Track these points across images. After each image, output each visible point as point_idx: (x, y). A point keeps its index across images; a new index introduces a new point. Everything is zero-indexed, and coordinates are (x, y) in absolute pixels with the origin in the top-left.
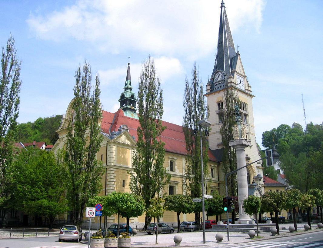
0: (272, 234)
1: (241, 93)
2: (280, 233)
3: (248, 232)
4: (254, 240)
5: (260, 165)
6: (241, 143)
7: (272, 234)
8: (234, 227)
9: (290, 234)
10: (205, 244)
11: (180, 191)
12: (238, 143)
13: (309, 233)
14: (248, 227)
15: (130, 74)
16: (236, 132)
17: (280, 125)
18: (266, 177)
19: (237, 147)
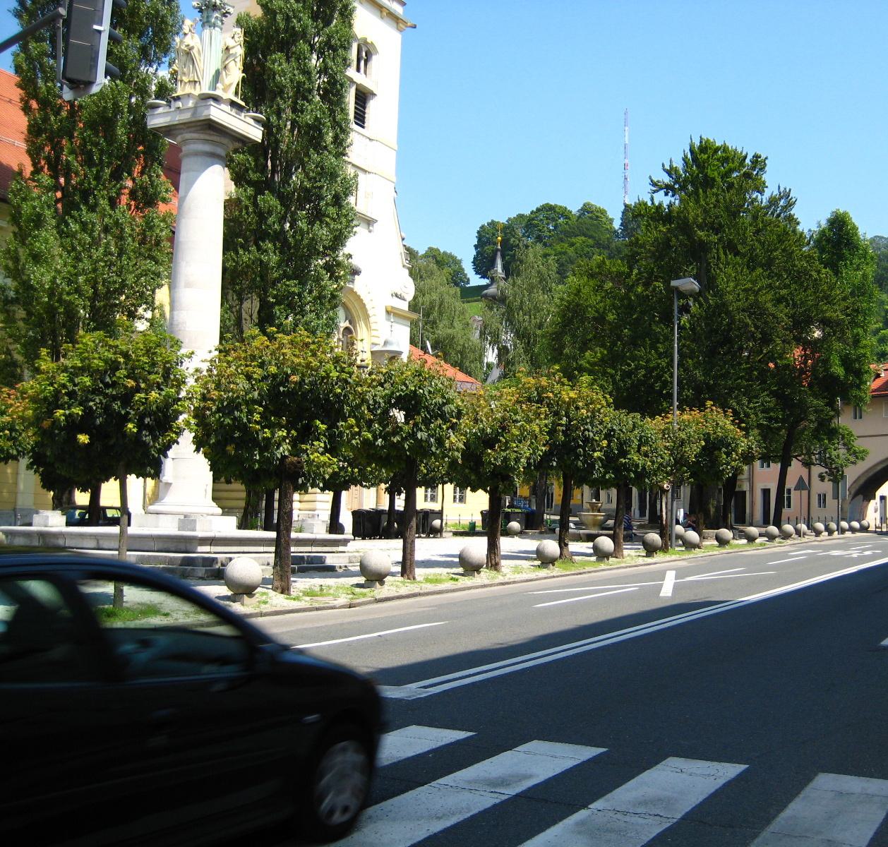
0: (230, 593)
1: (379, 13)
2: (503, 562)
3: (593, 541)
4: (674, 557)
5: (404, 306)
6: (203, 115)
7: (230, 593)
8: (105, 544)
9: (641, 561)
10: (818, 539)
11: (247, 387)
12: (186, 117)
13: (568, 575)
14: (172, 547)
15: (859, 477)
16: (184, 58)
17: (539, 206)
18: (427, 355)
19: (188, 136)
